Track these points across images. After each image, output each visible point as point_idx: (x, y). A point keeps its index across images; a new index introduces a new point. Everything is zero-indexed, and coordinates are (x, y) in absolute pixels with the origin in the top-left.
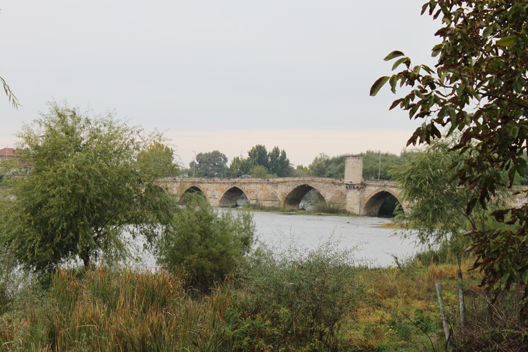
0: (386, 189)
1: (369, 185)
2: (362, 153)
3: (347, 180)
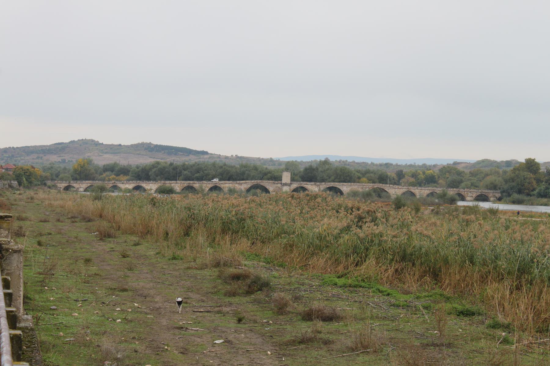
0: (140, 184)
1: (293, 184)
2: (535, 159)
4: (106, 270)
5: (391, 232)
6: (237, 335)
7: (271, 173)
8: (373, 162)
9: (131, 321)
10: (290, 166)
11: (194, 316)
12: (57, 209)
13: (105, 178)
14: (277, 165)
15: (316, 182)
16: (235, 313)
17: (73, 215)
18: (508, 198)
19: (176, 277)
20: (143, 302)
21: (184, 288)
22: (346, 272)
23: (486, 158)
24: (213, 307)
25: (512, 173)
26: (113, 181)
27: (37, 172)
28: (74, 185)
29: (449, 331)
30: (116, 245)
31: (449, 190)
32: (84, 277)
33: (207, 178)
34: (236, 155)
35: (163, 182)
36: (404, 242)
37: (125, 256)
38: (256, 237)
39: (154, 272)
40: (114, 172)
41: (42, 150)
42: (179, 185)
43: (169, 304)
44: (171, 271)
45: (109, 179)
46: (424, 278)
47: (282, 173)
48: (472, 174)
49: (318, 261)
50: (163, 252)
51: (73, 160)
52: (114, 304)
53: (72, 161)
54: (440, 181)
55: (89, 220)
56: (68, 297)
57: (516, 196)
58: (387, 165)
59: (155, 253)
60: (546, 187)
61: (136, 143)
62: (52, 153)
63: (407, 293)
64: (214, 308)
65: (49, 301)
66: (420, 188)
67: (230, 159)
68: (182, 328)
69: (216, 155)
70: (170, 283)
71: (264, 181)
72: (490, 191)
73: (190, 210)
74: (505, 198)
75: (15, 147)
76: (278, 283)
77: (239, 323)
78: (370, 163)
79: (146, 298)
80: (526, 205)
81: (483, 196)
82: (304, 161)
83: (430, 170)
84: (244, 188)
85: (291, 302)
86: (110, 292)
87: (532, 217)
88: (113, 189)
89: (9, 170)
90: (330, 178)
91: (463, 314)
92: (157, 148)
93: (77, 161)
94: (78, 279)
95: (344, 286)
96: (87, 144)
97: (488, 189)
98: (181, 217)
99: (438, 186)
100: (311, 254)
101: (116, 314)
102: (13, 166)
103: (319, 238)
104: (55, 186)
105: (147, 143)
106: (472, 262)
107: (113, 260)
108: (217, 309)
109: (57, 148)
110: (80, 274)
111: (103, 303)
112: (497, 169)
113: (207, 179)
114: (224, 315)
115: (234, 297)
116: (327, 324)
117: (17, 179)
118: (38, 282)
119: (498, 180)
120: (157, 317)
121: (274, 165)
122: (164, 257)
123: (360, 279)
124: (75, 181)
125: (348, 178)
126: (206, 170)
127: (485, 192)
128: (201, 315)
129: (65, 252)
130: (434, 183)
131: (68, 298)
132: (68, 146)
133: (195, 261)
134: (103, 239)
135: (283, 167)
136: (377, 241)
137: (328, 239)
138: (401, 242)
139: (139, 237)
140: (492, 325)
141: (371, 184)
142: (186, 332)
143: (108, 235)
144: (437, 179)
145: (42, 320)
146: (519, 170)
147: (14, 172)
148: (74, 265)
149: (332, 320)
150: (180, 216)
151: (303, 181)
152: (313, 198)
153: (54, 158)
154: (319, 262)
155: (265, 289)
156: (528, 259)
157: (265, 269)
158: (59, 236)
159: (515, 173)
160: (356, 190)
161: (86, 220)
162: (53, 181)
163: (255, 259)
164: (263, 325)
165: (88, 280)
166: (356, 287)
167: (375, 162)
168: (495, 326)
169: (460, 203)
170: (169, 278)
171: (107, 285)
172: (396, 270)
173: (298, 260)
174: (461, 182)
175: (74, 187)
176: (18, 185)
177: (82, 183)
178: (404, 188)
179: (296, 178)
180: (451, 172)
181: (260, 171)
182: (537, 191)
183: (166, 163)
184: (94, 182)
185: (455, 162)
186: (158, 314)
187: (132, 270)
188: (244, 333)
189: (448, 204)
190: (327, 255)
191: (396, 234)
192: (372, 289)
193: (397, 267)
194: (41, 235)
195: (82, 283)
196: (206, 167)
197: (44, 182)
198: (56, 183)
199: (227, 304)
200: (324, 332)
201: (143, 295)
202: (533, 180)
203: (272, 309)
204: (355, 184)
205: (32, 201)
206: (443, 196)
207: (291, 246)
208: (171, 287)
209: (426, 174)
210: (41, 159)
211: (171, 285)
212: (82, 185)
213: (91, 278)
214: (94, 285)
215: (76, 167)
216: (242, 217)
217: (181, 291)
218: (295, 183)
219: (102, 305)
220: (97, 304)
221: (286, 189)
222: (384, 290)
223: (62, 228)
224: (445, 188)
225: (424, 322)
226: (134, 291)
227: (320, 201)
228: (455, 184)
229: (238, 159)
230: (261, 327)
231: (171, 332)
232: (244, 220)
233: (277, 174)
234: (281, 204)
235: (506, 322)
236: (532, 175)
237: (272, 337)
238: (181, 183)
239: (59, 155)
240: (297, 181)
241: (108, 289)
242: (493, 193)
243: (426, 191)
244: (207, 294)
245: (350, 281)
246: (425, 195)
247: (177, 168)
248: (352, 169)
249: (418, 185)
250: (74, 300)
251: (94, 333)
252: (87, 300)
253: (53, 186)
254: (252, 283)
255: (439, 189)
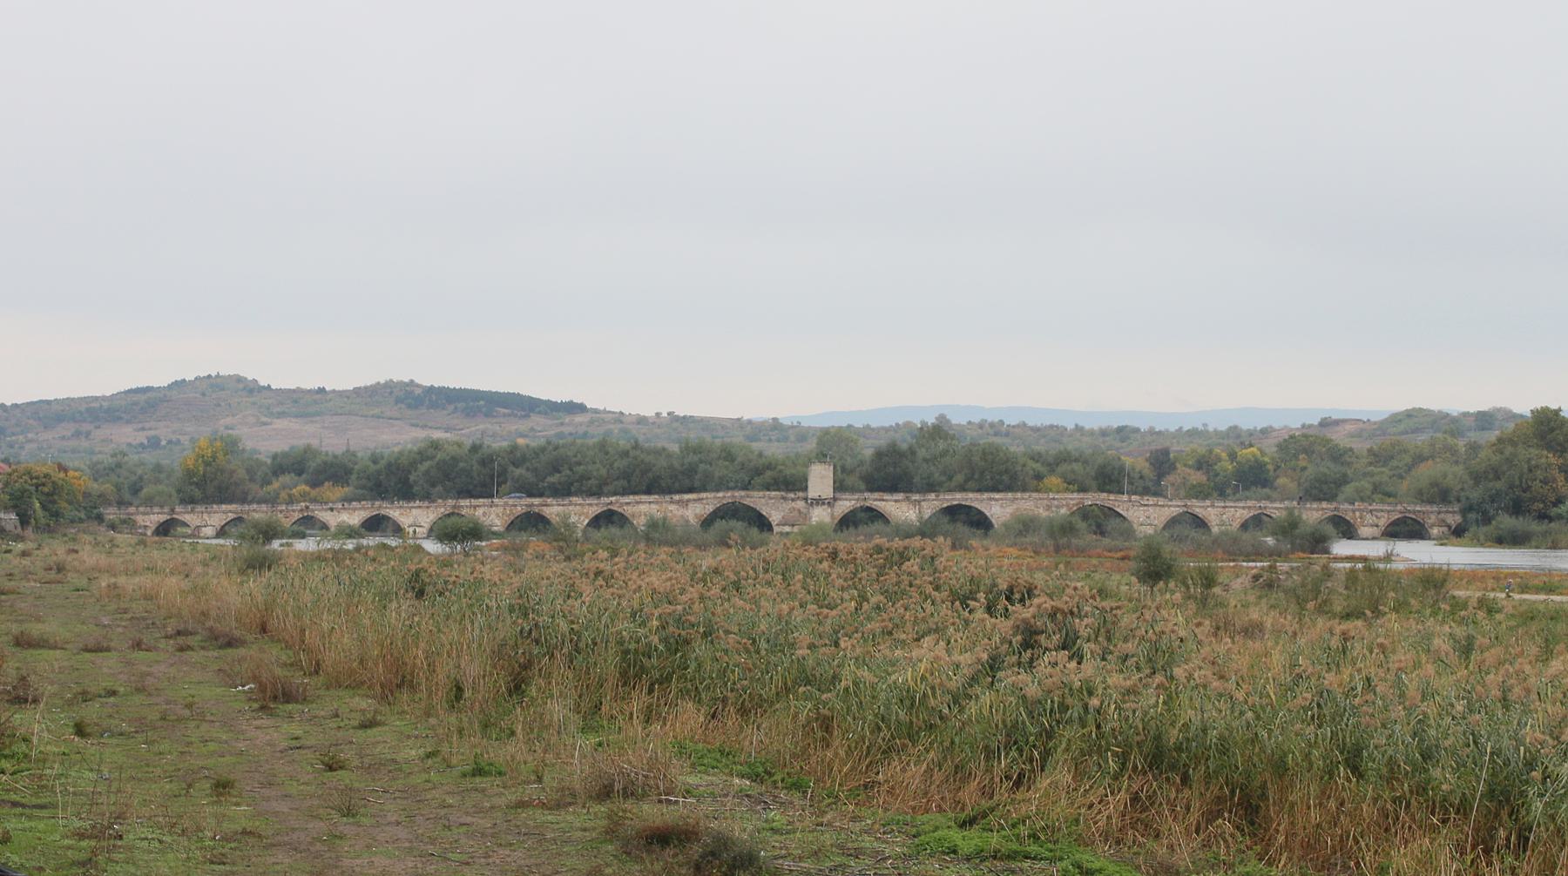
1: (840, 500)
3: (813, 493)
4: (276, 814)
13: (278, 494)
14: (792, 438)
15: (911, 491)
17: (181, 627)
18: (1484, 529)
19: (483, 835)
22: (985, 804)
26: (303, 504)
28: (187, 518)
30: (307, 728)
31: (1308, 506)
35: (451, 502)
37: (334, 765)
38: (722, 693)
39: (419, 819)
40: (304, 476)
41: (88, 410)
44: (467, 814)
45: (290, 495)
46: (1214, 825)
47: (807, 467)
48: (1374, 455)
49: (904, 770)
50: (445, 749)
54: (1281, 481)
55: (231, 643)
57: (1506, 522)
58: (1123, 433)
62: (121, 418)
67: (654, 423)
69: (609, 412)
70: (464, 858)
71: (755, 494)
72: (1428, 508)
73: (526, 615)
74: (1473, 529)
76: (783, 852)
78: (1070, 426)
80: (1537, 547)
83: (1251, 446)
84: (696, 515)
88: (302, 528)
90: (950, 478)
92: (434, 397)
93: (192, 440)
94: (193, 847)
97: (1423, 501)
99: (1275, 495)
100: (884, 752)
103: (907, 703)
104: (129, 524)
105: (401, 383)
107: (298, 781)
109: (136, 404)
110: (200, 834)
113: (583, 492)
117: (15, 507)
118: (74, 863)
119: (1453, 473)
121: (786, 439)
122: (448, 766)
123: (1024, 831)
124: (189, 507)
126: (579, 464)
127: (1414, 512)
129: (156, 754)
130: (1264, 486)
132: (165, 396)
133: (540, 779)
135: (811, 445)
136: (1075, 712)
137: (932, 702)
139: (374, 697)
141: (1075, 495)
144: (1271, 473)
146: (1514, 444)
148: (183, 798)
150: (497, 634)
151: (871, 490)
152: (896, 557)
153: (126, 436)
154: (909, 774)
158: (138, 699)
159: (1502, 453)
160: (1030, 513)
161: (221, 640)
162: (123, 508)
166: (1014, 859)
169: (1342, 548)
170: (463, 841)
172: (1135, 799)
174: (1343, 481)
175: (185, 525)
176: (18, 524)
177: (209, 513)
178: (1174, 503)
179: (851, 480)
180: (1313, 452)
183: (459, 445)
184: (246, 507)
185: (1326, 418)
187: (353, 816)
189: (1304, 551)
190: (932, 754)
191: (1135, 685)
193: (1135, 787)
194: (85, 696)
196: (579, 456)
197: (95, 511)
198: (132, 514)
202: (1556, 473)
204: (1026, 495)
206: (1288, 528)
207: (826, 724)
210: (87, 437)
211: (468, 864)
213: (233, 845)
215: (190, 463)
216: (679, 635)
218: (847, 496)
221: (820, 515)
224: (1295, 503)
227: (916, 568)
228: (1325, 487)
229: (675, 425)
232: (687, 642)
233: (793, 471)
234: (799, 581)
236: (1552, 459)
238: (506, 504)
239: (140, 426)
240: (853, 490)
242: (1439, 513)
243: (1240, 511)
245: (994, 840)
246: (1236, 525)
247: (492, 461)
248: (1016, 449)
249: (1215, 495)
253: (124, 522)
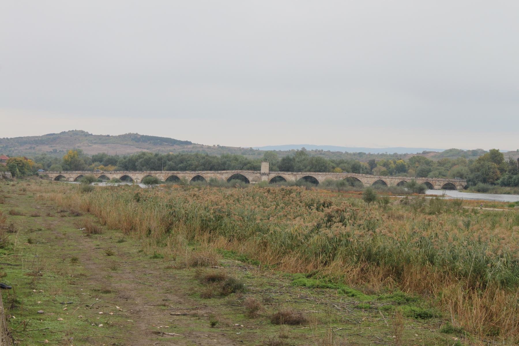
0: (127, 174)
1: (271, 174)
2: (499, 150)
3: (262, 171)
5: (357, 232)
6: (210, 340)
7: (251, 163)
8: (347, 151)
9: (112, 326)
10: (269, 156)
11: (171, 320)
12: (48, 202)
13: (94, 168)
14: (256, 154)
15: (293, 171)
16: (210, 317)
17: (62, 209)
18: (474, 187)
20: (124, 304)
21: (163, 289)
22: (315, 270)
23: (454, 148)
24: (189, 310)
25: (477, 163)
27: (29, 163)
28: (65, 175)
29: (406, 335)
31: (418, 179)
32: (71, 278)
33: (190, 168)
34: (218, 145)
35: (148, 172)
36: (369, 243)
37: (110, 254)
39: (136, 272)
40: (102, 163)
41: (34, 140)
42: (164, 174)
43: (149, 307)
44: (151, 270)
47: (261, 163)
48: (440, 163)
49: (289, 259)
50: (145, 250)
51: (64, 150)
52: (97, 307)
53: (63, 151)
54: (410, 171)
55: (78, 215)
56: (54, 301)
57: (481, 185)
58: (360, 154)
59: (138, 250)
60: (509, 176)
61: (123, 134)
63: (371, 293)
64: (190, 310)
65: (36, 304)
66: (391, 178)
67: (213, 148)
68: (159, 333)
69: (199, 145)
71: (244, 171)
73: (171, 208)
74: (470, 187)
75: (9, 138)
76: (251, 284)
77: (212, 327)
79: (127, 300)
80: (491, 193)
81: (450, 184)
82: (282, 150)
83: (401, 159)
85: (262, 306)
86: (94, 294)
87: (494, 207)
88: (101, 179)
89: (3, 161)
90: (306, 168)
91: (421, 317)
93: (67, 151)
94: (65, 279)
95: (312, 287)
96: (77, 135)
98: (163, 214)
99: (408, 175)
101: (98, 318)
102: (7, 157)
104: (47, 176)
106: (432, 263)
107: (98, 259)
108: (193, 312)
111: (87, 306)
112: (464, 159)
114: (199, 319)
115: (209, 299)
116: (294, 328)
117: (11, 170)
118: (27, 283)
119: (464, 170)
120: (136, 321)
121: (254, 154)
122: (146, 255)
123: (327, 279)
124: (66, 172)
125: (323, 168)
126: (189, 161)
127: (452, 181)
128: (177, 318)
129: (54, 249)
130: (404, 172)
131: (55, 301)
132: (59, 136)
133: (175, 260)
134: (90, 236)
135: (262, 156)
136: (344, 242)
137: (299, 238)
138: (366, 243)
139: (123, 233)
140: (446, 330)
142: (163, 338)
143: (95, 231)
144: (407, 168)
145: (29, 325)
146: (484, 160)
147: (8, 163)
148: (62, 264)
149: (299, 323)
151: (281, 171)
152: (288, 192)
153: (46, 149)
155: (238, 291)
156: (483, 261)
157: (239, 268)
159: (480, 163)
161: (75, 214)
163: (231, 256)
164: (234, 329)
165: (74, 280)
166: (324, 288)
167: (350, 152)
168: (449, 331)
169: (429, 192)
171: (91, 286)
172: (362, 270)
173: (271, 259)
174: (430, 171)
175: (64, 177)
177: (72, 174)
178: (376, 177)
179: (274, 168)
180: (420, 162)
181: (241, 162)
182: (501, 180)
183: (151, 154)
184: (84, 172)
186: (138, 317)
188: (216, 338)
189: (417, 193)
190: (298, 254)
191: (363, 234)
192: (338, 290)
193: (362, 266)
194: (32, 231)
195: (68, 284)
196: (189, 158)
198: (48, 173)
199: (203, 306)
200: (291, 336)
201: (125, 297)
202: (497, 170)
203: (244, 312)
204: (330, 173)
205: (24, 193)
206: (412, 186)
208: (151, 288)
209: (397, 163)
210: (34, 149)
211: (151, 286)
212: (72, 175)
213: (77, 279)
214: (79, 286)
216: (220, 215)
217: (161, 292)
218: (273, 172)
219: (86, 308)
220: (81, 307)
221: (265, 178)
222: (350, 290)
223: (52, 222)
224: (414, 178)
225: (384, 327)
226: (116, 292)
227: (294, 196)
228: (424, 173)
230: (232, 331)
231: (149, 338)
232: (222, 217)
233: (256, 164)
234: (258, 199)
235: (459, 327)
236: (496, 165)
237: (242, 342)
238: (166, 173)
239: (51, 146)
240: (275, 171)
241: (92, 290)
242: (460, 182)
244: (184, 295)
245: (317, 282)
246: (396, 184)
247: (162, 159)
248: (327, 159)
249: (389, 174)
250: (60, 303)
251: (77, 339)
252: (72, 303)
253: (45, 176)
254: (226, 285)
255: (408, 178)
